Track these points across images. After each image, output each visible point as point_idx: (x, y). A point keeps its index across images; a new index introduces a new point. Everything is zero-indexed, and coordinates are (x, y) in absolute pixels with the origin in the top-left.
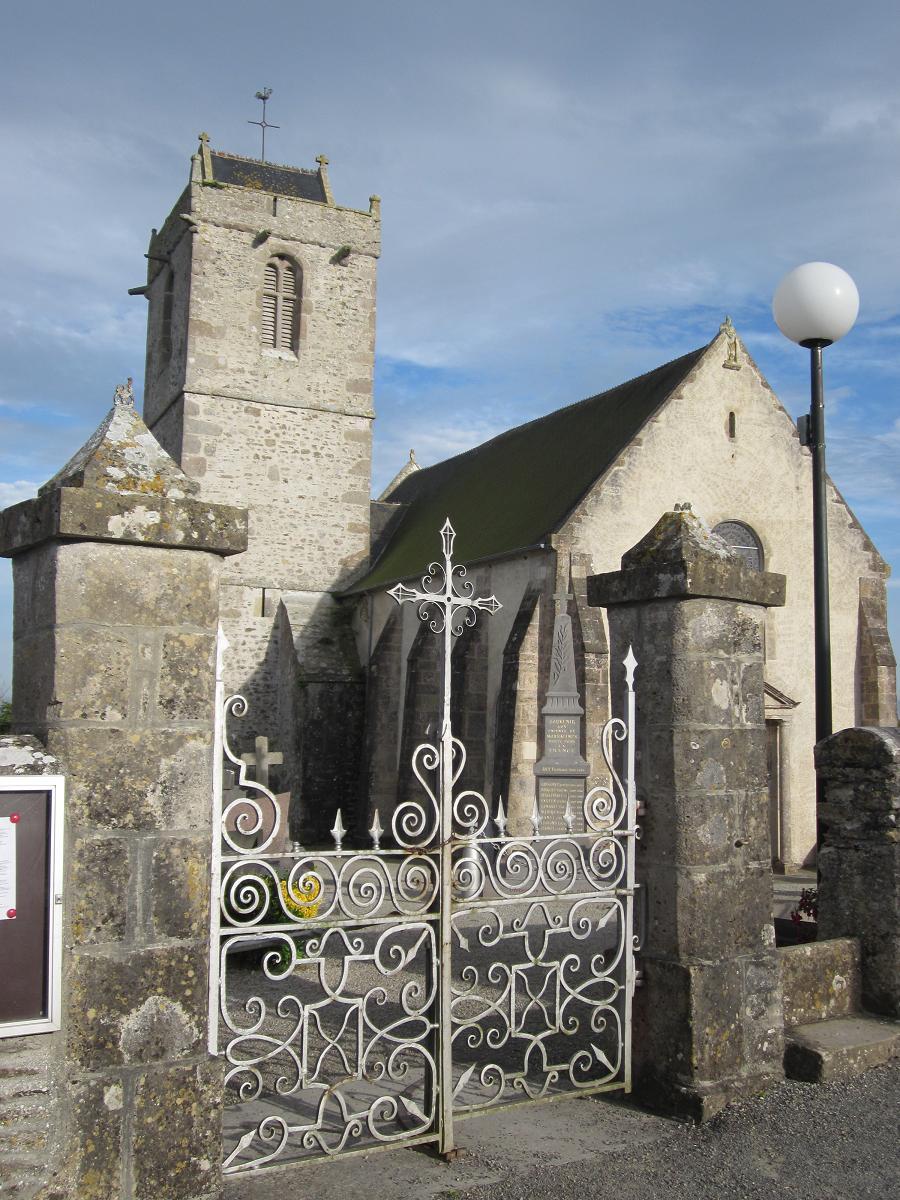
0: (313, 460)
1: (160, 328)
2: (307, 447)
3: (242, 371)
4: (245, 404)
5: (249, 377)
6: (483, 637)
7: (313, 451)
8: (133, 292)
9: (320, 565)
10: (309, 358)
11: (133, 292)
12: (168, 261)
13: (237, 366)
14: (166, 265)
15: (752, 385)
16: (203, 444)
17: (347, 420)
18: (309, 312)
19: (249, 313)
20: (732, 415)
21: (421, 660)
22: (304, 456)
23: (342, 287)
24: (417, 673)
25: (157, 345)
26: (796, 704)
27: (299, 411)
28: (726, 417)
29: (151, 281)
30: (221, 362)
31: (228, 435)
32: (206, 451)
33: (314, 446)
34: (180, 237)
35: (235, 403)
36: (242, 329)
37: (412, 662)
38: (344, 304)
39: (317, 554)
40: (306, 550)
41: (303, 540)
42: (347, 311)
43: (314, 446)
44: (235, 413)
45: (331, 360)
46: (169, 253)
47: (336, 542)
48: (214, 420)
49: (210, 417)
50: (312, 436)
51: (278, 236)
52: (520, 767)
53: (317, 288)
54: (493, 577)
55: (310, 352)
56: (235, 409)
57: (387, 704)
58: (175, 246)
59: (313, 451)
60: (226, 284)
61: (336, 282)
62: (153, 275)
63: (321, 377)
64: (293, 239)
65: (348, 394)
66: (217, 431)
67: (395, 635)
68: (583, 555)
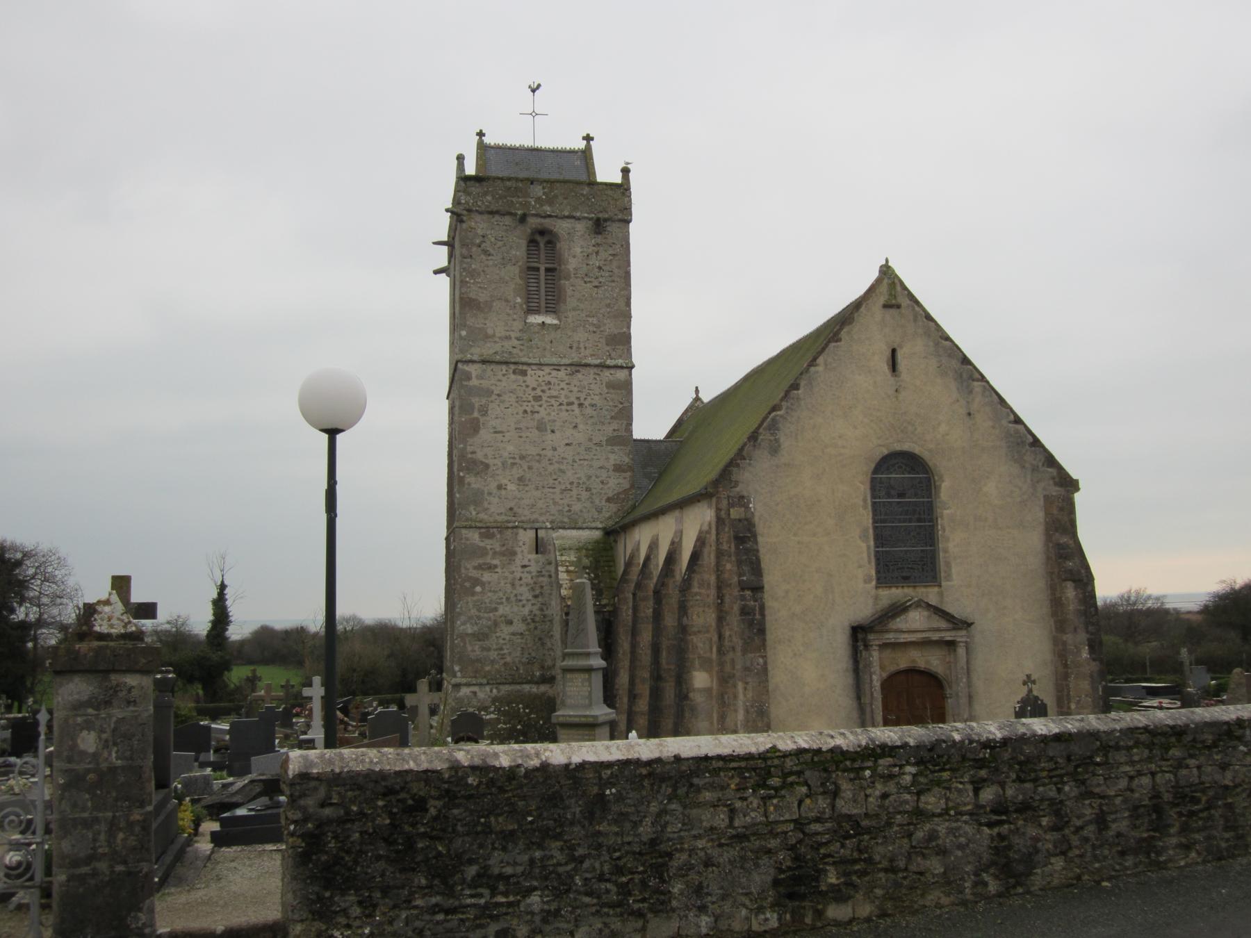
0: (577, 411)
2: (573, 399)
4: (513, 367)
5: (516, 343)
7: (576, 402)
8: (436, 272)
9: (588, 504)
10: (570, 320)
11: (436, 272)
13: (503, 334)
17: (607, 373)
18: (567, 278)
20: (894, 351)
23: (597, 253)
28: (888, 353)
30: (490, 332)
31: (499, 395)
32: (479, 411)
33: (578, 398)
35: (504, 367)
36: (507, 301)
39: (585, 495)
40: (574, 492)
41: (572, 483)
43: (578, 398)
51: (537, 215)
52: (691, 695)
55: (570, 314)
61: (591, 249)
63: (581, 335)
64: (550, 216)
66: (489, 392)
68: (743, 497)
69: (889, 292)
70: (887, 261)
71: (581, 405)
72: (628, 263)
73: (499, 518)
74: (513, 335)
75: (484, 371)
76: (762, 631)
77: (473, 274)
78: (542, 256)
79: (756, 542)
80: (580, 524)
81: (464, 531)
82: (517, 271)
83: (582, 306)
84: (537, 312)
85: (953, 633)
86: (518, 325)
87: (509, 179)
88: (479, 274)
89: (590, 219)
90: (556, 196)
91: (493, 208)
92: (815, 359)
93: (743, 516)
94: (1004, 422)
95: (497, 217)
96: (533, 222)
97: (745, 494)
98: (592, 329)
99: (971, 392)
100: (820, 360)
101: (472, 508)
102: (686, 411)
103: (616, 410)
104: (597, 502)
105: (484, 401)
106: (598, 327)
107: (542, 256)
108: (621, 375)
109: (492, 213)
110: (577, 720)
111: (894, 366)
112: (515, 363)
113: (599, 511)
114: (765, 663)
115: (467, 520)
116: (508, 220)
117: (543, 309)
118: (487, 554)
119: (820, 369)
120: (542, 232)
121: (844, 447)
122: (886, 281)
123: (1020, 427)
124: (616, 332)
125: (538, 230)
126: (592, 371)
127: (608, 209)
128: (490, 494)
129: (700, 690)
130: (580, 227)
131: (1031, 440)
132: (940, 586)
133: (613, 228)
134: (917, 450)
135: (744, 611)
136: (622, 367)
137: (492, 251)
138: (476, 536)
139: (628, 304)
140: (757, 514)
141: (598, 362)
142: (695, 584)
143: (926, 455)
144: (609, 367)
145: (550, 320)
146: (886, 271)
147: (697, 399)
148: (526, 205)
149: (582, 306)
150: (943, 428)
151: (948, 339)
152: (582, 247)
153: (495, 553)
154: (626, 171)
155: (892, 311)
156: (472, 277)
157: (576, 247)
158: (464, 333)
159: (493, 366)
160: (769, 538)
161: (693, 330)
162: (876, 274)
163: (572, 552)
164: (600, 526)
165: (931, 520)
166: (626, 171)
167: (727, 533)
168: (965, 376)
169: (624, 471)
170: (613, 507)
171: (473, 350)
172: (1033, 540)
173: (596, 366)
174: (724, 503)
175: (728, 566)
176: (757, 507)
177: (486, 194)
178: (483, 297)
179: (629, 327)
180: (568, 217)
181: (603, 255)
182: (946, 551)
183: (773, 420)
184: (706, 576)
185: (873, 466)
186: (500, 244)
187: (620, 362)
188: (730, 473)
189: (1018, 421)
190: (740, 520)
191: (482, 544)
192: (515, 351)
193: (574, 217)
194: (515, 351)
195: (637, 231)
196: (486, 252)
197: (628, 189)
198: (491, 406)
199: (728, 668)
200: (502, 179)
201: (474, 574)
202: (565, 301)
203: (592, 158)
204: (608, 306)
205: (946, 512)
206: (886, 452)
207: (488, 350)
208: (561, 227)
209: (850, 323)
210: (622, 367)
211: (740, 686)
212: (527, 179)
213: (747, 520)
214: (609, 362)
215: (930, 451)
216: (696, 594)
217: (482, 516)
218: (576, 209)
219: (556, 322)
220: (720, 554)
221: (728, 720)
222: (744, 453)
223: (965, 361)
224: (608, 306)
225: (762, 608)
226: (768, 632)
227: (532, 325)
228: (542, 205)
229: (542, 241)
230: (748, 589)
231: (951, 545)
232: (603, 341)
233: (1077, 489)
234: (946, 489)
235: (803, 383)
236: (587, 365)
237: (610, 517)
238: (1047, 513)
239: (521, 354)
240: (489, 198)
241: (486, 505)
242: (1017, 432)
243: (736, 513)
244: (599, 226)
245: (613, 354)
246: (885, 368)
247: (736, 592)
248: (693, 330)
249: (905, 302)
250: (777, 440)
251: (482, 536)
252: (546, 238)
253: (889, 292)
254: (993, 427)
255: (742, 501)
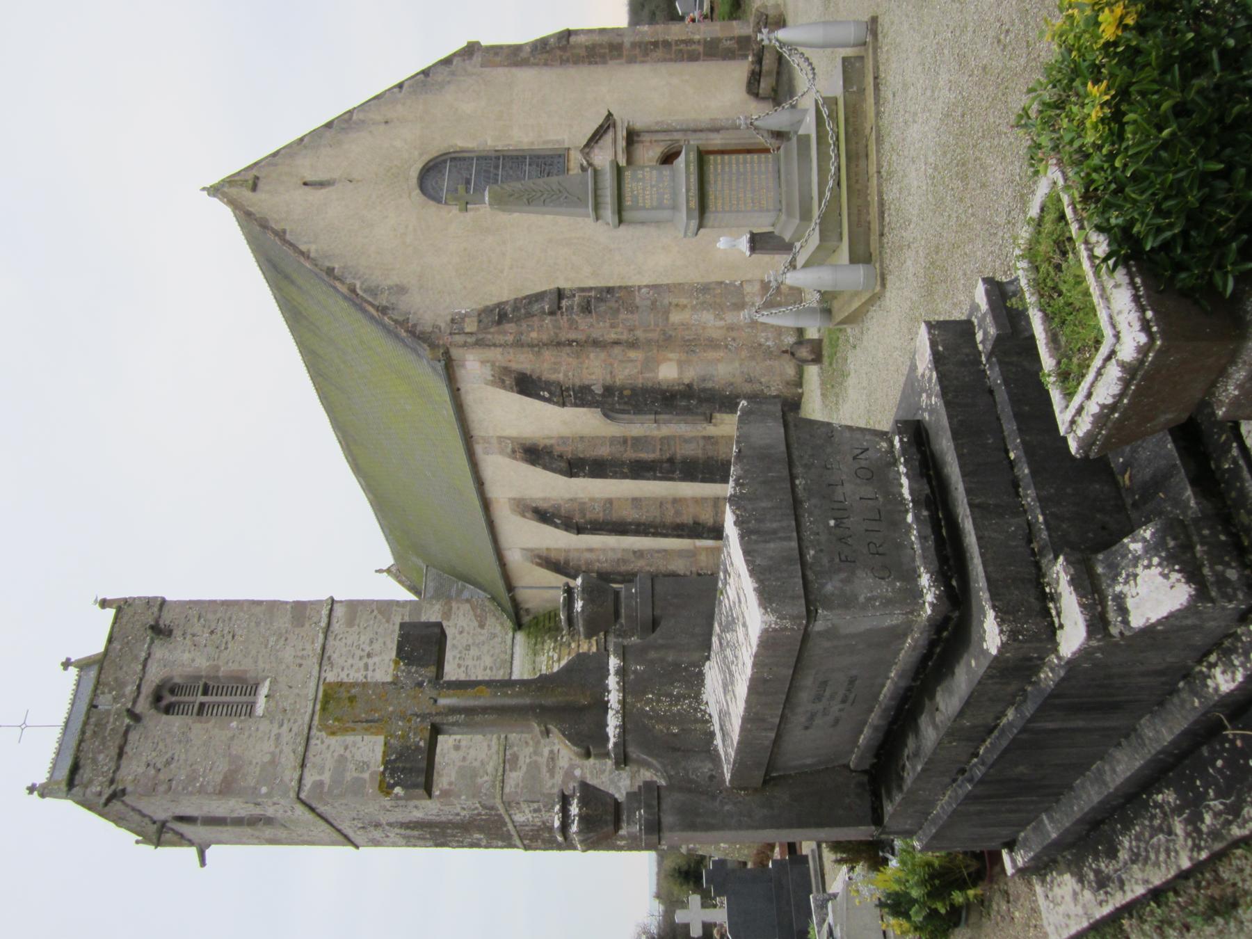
0: (376, 659)
1: (238, 830)
2: (361, 664)
3: (278, 736)
4: (314, 731)
5: (285, 728)
6: (548, 442)
7: (365, 660)
8: (203, 863)
9: (485, 648)
10: (267, 667)
11: (203, 863)
12: (164, 824)
13: (272, 742)
14: (169, 825)
15: (276, 165)
16: (355, 774)
17: (336, 626)
18: (217, 668)
19: (216, 730)
20: (305, 184)
21: (578, 518)
22: (371, 668)
23: (194, 635)
24: (591, 522)
25: (257, 833)
26: (610, 115)
27: (323, 675)
28: (307, 188)
29: (191, 843)
30: (267, 758)
31: (346, 748)
32: (363, 771)
33: (361, 658)
34: (134, 809)
35: (313, 742)
36: (232, 738)
37: (580, 530)
38: (212, 632)
39: (474, 652)
40: (470, 662)
41: (459, 666)
42: (219, 629)
43: (361, 658)
44: (323, 742)
45: (271, 643)
46: (154, 822)
47: (461, 633)
48: (330, 764)
49: (327, 768)
50: (350, 661)
51: (135, 702)
52: (687, 381)
53: (193, 660)
54: (483, 434)
55: (261, 665)
56: (319, 742)
57: (625, 561)
58: (144, 816)
59: (365, 660)
60: (183, 757)
61: (188, 642)
62: (182, 840)
63: (288, 654)
64: (139, 687)
65: (307, 625)
66: (342, 760)
67: (553, 555)
68: (453, 320)
69: (241, 191)
70: (204, 189)
71: (369, 655)
72: (212, 603)
73: (495, 748)
74: (275, 731)
75: (314, 765)
76: (609, 290)
77: (192, 778)
78: (187, 699)
79: (507, 302)
80: (508, 657)
81: (507, 790)
82: (199, 725)
83: (254, 652)
84: (252, 705)
85: (619, 129)
86: (264, 726)
87: (83, 732)
88: (194, 771)
89: (152, 641)
90: (116, 679)
91: (114, 752)
92: (302, 253)
93: (475, 319)
94: (400, 96)
95: (127, 749)
96: (142, 706)
97: (449, 318)
98: (282, 642)
99: (363, 121)
100: (303, 248)
101: (479, 781)
102: (401, 582)
103: (379, 617)
104: (482, 638)
105: (352, 766)
106: (280, 636)
107: (187, 699)
108: (339, 612)
109: (120, 754)
110: (694, 179)
111: (321, 184)
112: (310, 728)
113: (494, 636)
114: (647, 286)
115: (494, 786)
116: (133, 736)
117: (251, 699)
118: (536, 762)
119: (313, 247)
120: (157, 698)
121: (407, 227)
122: (226, 189)
123: (406, 86)
124: (289, 615)
125: (158, 722)
126: (331, 642)
127: (145, 623)
128: (464, 759)
129: (681, 372)
130: (160, 652)
131: (422, 76)
132: (569, 149)
133: (166, 619)
134: (420, 165)
135: (586, 308)
136: (331, 610)
137: (169, 755)
138: (514, 775)
139: (259, 603)
140: (474, 307)
141: (321, 636)
142: (553, 377)
143: (426, 158)
144: (329, 624)
145: (264, 690)
146: (215, 191)
147: (388, 571)
148: (118, 714)
149: (254, 652)
150: (398, 143)
151: (302, 139)
152: (184, 651)
153: (535, 753)
154: (104, 604)
155: (261, 185)
156: (195, 779)
157: (180, 659)
158: (264, 790)
159: (310, 754)
160: (503, 291)
161: (297, 529)
162: (216, 200)
163: (538, 659)
164: (511, 634)
165: (498, 158)
166: (104, 604)
167: (493, 335)
168: (344, 126)
169: (450, 609)
170: (491, 621)
171: (286, 779)
172: (525, 76)
173: (326, 638)
174: (459, 339)
175: (534, 335)
176: (465, 306)
177: (94, 761)
178: (223, 766)
179: (287, 603)
180: (144, 666)
181: (197, 628)
182: (533, 143)
183: (365, 291)
184: (546, 365)
185: (431, 203)
186: (161, 746)
187: (325, 612)
188: (422, 333)
189: (400, 86)
190: (480, 321)
191: (524, 768)
192: (295, 729)
193: (146, 659)
194: (295, 729)
195: (174, 593)
196: (168, 763)
197: (126, 601)
198: (358, 757)
199: (654, 335)
200: (81, 741)
201: (559, 778)
202: (245, 672)
203: (90, 658)
204: (258, 624)
205: (489, 143)
206: (418, 191)
207: (289, 761)
208: (155, 674)
209: (267, 220)
210: (331, 610)
211: (675, 317)
212: (89, 711)
213: (479, 315)
214: (323, 624)
215: (421, 155)
216: (566, 375)
217: (490, 768)
218: (136, 658)
219: (267, 683)
220: (518, 344)
221: (714, 336)
222: (401, 319)
223: (329, 125)
224: (258, 624)
225: (583, 290)
226: (611, 284)
227: (266, 709)
228: (123, 696)
229: (169, 699)
230: (559, 302)
231: (526, 140)
232: (297, 630)
233: (478, 43)
234: (462, 142)
235: (328, 264)
236: (324, 648)
237: (502, 624)
238: (500, 65)
239: (300, 722)
240: (101, 757)
241: (476, 764)
242: (410, 86)
243: (471, 326)
244: (160, 631)
245: (315, 619)
246: (324, 191)
247: (563, 321)
248: (297, 529)
249: (255, 172)
250: (390, 288)
251: (514, 768)
252: (166, 694)
253: (241, 191)
254: (404, 104)
255: (456, 321)
